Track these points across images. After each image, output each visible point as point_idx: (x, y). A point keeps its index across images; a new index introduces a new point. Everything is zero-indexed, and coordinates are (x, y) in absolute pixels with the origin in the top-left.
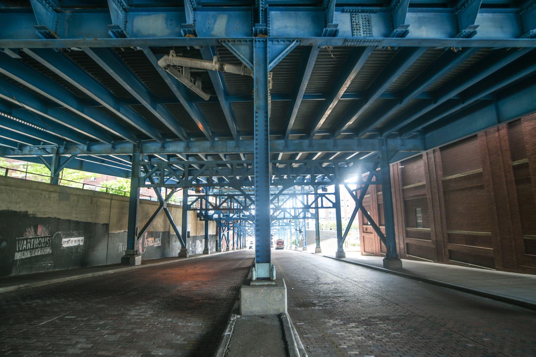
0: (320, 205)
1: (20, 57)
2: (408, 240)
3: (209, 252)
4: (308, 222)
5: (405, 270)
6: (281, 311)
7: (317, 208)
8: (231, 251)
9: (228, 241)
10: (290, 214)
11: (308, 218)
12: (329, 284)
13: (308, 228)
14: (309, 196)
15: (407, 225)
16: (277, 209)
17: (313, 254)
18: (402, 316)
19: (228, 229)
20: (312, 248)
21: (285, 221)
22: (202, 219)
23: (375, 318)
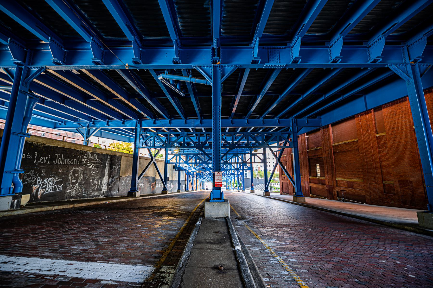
0: (253, 161)
1: (79, 73)
2: (311, 185)
3: (181, 191)
4: (246, 173)
5: (307, 203)
6: (227, 215)
7: (251, 163)
8: (194, 191)
9: (193, 184)
10: (234, 167)
11: (246, 170)
12: (257, 209)
13: (246, 177)
14: (246, 155)
15: (310, 176)
16: (226, 162)
17: (249, 193)
18: (298, 224)
19: (193, 177)
20: (248, 191)
21: (231, 171)
22: (177, 169)
23: (282, 225)
